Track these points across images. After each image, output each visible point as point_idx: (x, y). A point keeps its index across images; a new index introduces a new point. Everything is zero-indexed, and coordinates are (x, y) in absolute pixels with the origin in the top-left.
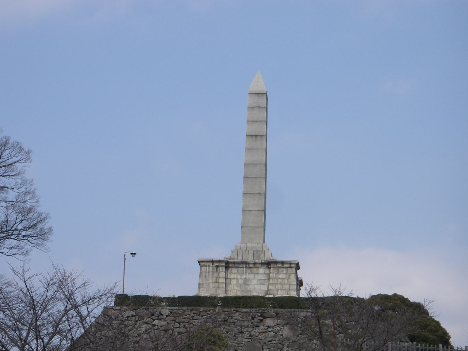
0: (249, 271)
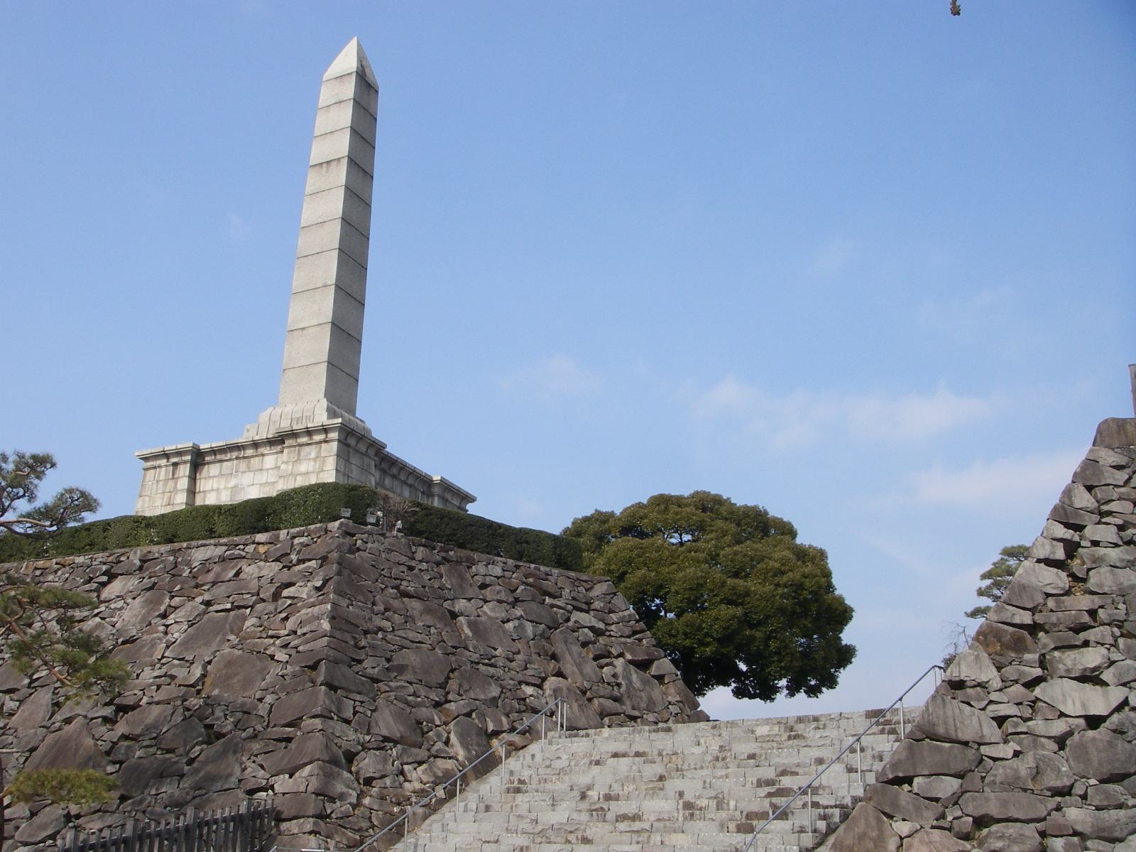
0: (243, 465)
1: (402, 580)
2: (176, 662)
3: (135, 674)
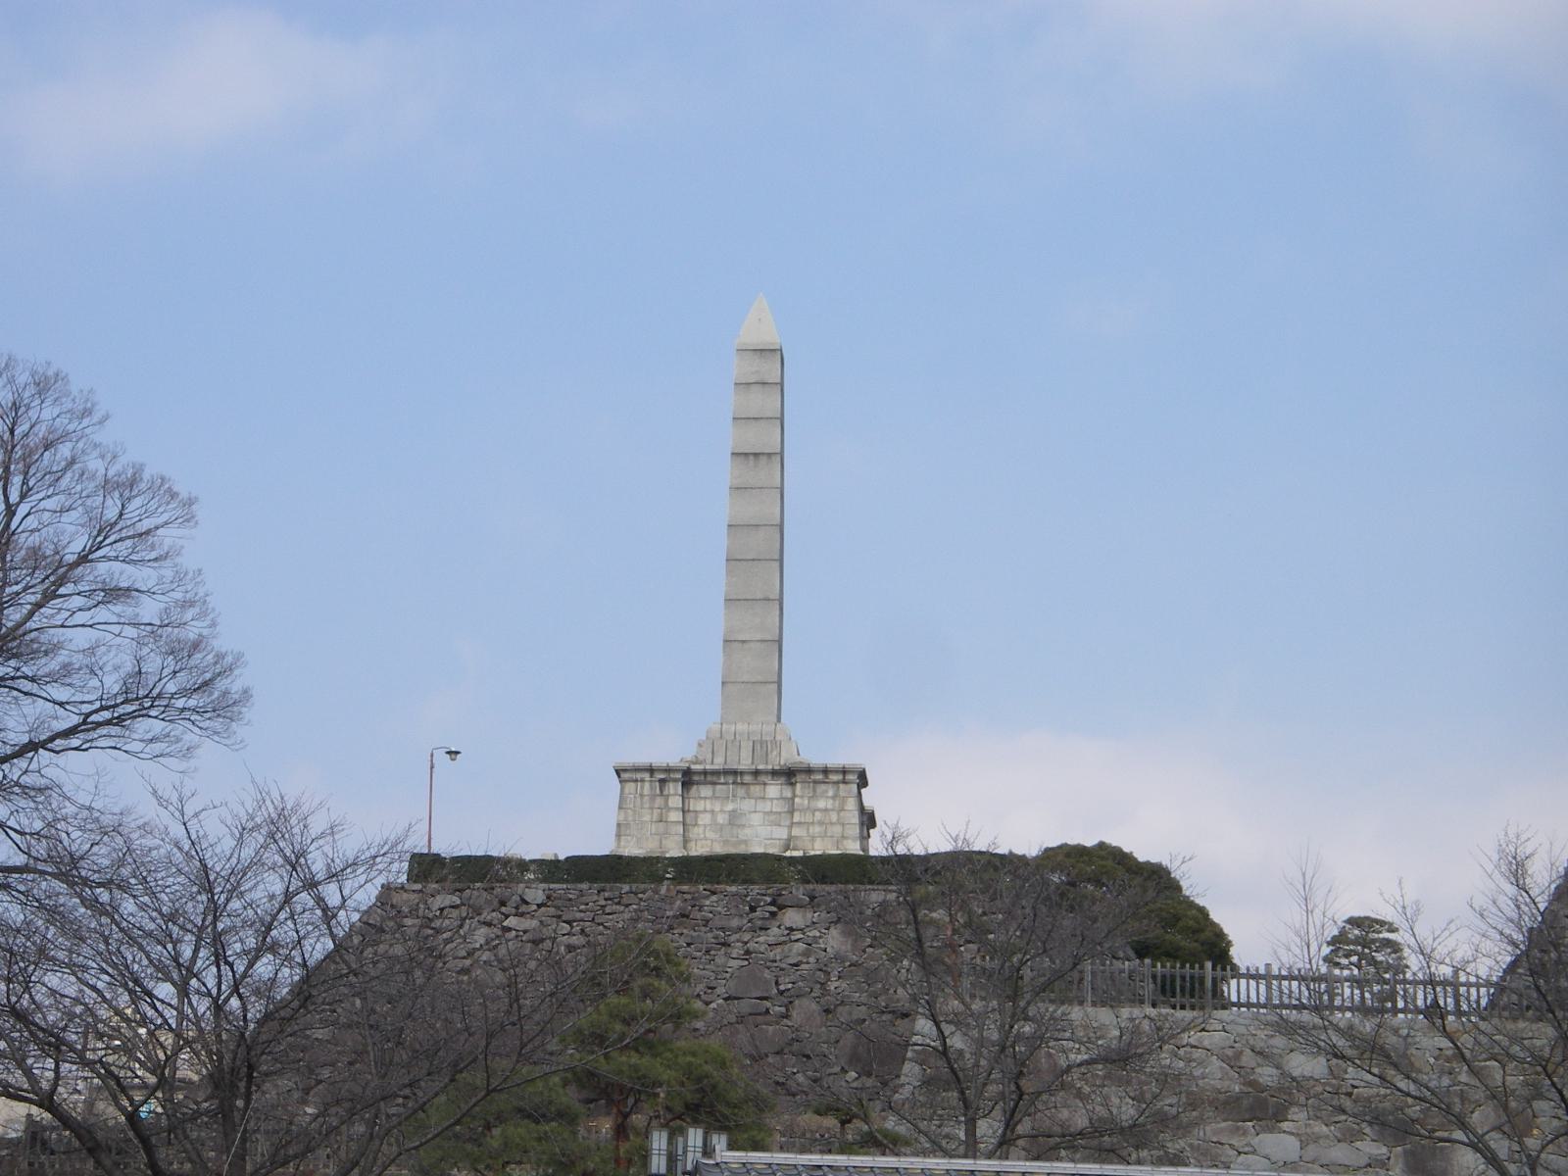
0: (741, 791)
3: (323, 978)
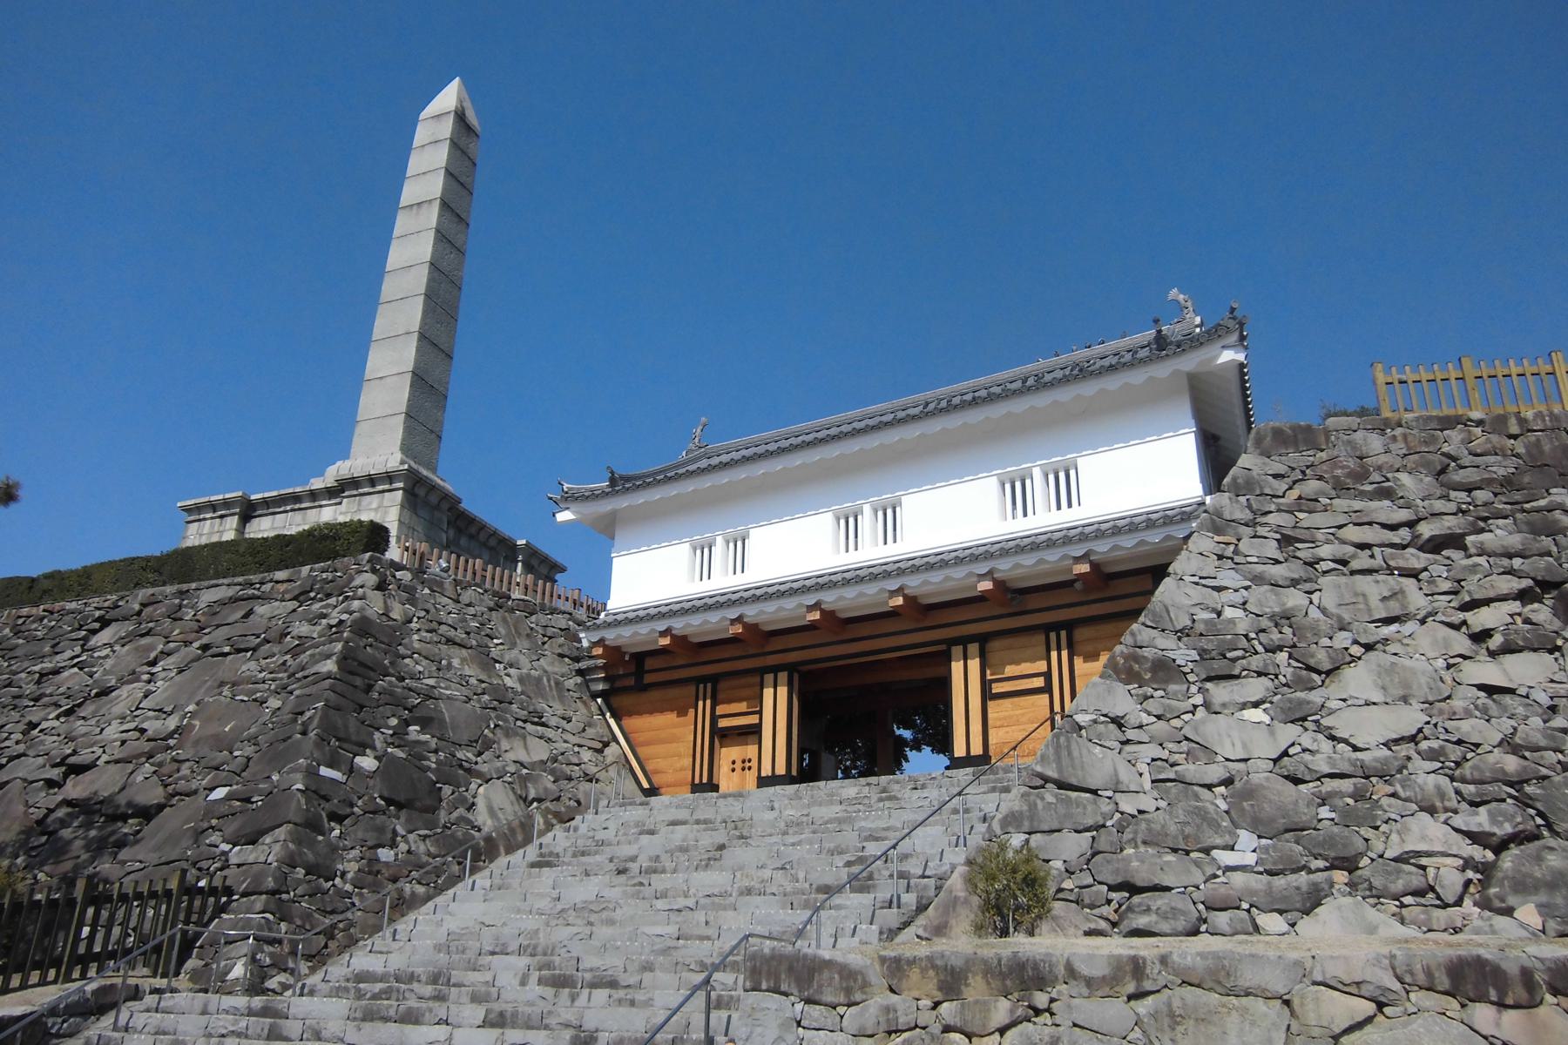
1: (440, 624)
2: (151, 714)
